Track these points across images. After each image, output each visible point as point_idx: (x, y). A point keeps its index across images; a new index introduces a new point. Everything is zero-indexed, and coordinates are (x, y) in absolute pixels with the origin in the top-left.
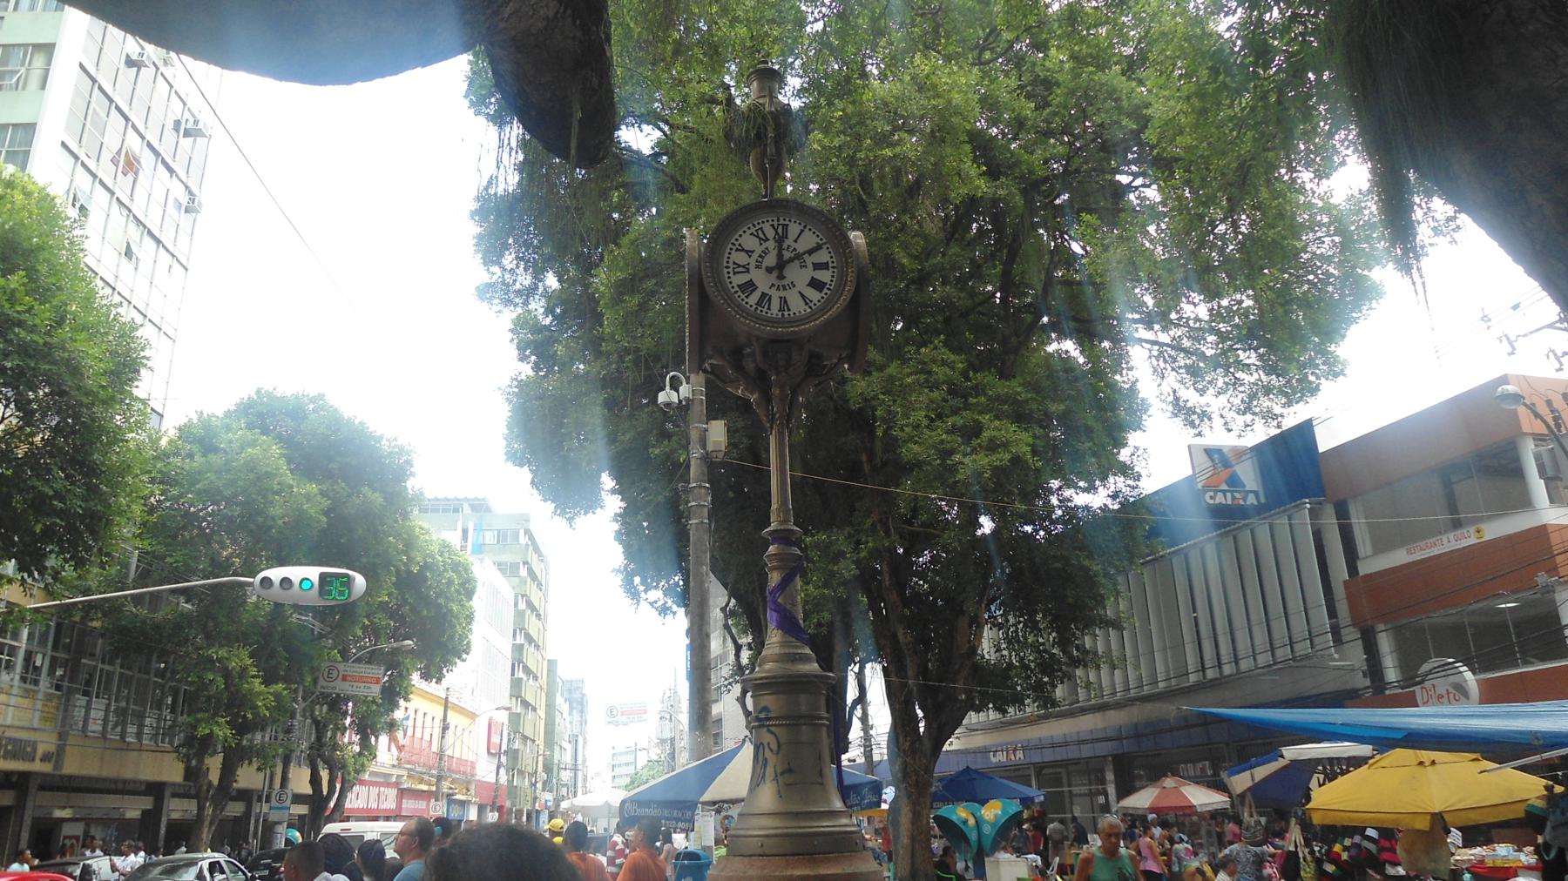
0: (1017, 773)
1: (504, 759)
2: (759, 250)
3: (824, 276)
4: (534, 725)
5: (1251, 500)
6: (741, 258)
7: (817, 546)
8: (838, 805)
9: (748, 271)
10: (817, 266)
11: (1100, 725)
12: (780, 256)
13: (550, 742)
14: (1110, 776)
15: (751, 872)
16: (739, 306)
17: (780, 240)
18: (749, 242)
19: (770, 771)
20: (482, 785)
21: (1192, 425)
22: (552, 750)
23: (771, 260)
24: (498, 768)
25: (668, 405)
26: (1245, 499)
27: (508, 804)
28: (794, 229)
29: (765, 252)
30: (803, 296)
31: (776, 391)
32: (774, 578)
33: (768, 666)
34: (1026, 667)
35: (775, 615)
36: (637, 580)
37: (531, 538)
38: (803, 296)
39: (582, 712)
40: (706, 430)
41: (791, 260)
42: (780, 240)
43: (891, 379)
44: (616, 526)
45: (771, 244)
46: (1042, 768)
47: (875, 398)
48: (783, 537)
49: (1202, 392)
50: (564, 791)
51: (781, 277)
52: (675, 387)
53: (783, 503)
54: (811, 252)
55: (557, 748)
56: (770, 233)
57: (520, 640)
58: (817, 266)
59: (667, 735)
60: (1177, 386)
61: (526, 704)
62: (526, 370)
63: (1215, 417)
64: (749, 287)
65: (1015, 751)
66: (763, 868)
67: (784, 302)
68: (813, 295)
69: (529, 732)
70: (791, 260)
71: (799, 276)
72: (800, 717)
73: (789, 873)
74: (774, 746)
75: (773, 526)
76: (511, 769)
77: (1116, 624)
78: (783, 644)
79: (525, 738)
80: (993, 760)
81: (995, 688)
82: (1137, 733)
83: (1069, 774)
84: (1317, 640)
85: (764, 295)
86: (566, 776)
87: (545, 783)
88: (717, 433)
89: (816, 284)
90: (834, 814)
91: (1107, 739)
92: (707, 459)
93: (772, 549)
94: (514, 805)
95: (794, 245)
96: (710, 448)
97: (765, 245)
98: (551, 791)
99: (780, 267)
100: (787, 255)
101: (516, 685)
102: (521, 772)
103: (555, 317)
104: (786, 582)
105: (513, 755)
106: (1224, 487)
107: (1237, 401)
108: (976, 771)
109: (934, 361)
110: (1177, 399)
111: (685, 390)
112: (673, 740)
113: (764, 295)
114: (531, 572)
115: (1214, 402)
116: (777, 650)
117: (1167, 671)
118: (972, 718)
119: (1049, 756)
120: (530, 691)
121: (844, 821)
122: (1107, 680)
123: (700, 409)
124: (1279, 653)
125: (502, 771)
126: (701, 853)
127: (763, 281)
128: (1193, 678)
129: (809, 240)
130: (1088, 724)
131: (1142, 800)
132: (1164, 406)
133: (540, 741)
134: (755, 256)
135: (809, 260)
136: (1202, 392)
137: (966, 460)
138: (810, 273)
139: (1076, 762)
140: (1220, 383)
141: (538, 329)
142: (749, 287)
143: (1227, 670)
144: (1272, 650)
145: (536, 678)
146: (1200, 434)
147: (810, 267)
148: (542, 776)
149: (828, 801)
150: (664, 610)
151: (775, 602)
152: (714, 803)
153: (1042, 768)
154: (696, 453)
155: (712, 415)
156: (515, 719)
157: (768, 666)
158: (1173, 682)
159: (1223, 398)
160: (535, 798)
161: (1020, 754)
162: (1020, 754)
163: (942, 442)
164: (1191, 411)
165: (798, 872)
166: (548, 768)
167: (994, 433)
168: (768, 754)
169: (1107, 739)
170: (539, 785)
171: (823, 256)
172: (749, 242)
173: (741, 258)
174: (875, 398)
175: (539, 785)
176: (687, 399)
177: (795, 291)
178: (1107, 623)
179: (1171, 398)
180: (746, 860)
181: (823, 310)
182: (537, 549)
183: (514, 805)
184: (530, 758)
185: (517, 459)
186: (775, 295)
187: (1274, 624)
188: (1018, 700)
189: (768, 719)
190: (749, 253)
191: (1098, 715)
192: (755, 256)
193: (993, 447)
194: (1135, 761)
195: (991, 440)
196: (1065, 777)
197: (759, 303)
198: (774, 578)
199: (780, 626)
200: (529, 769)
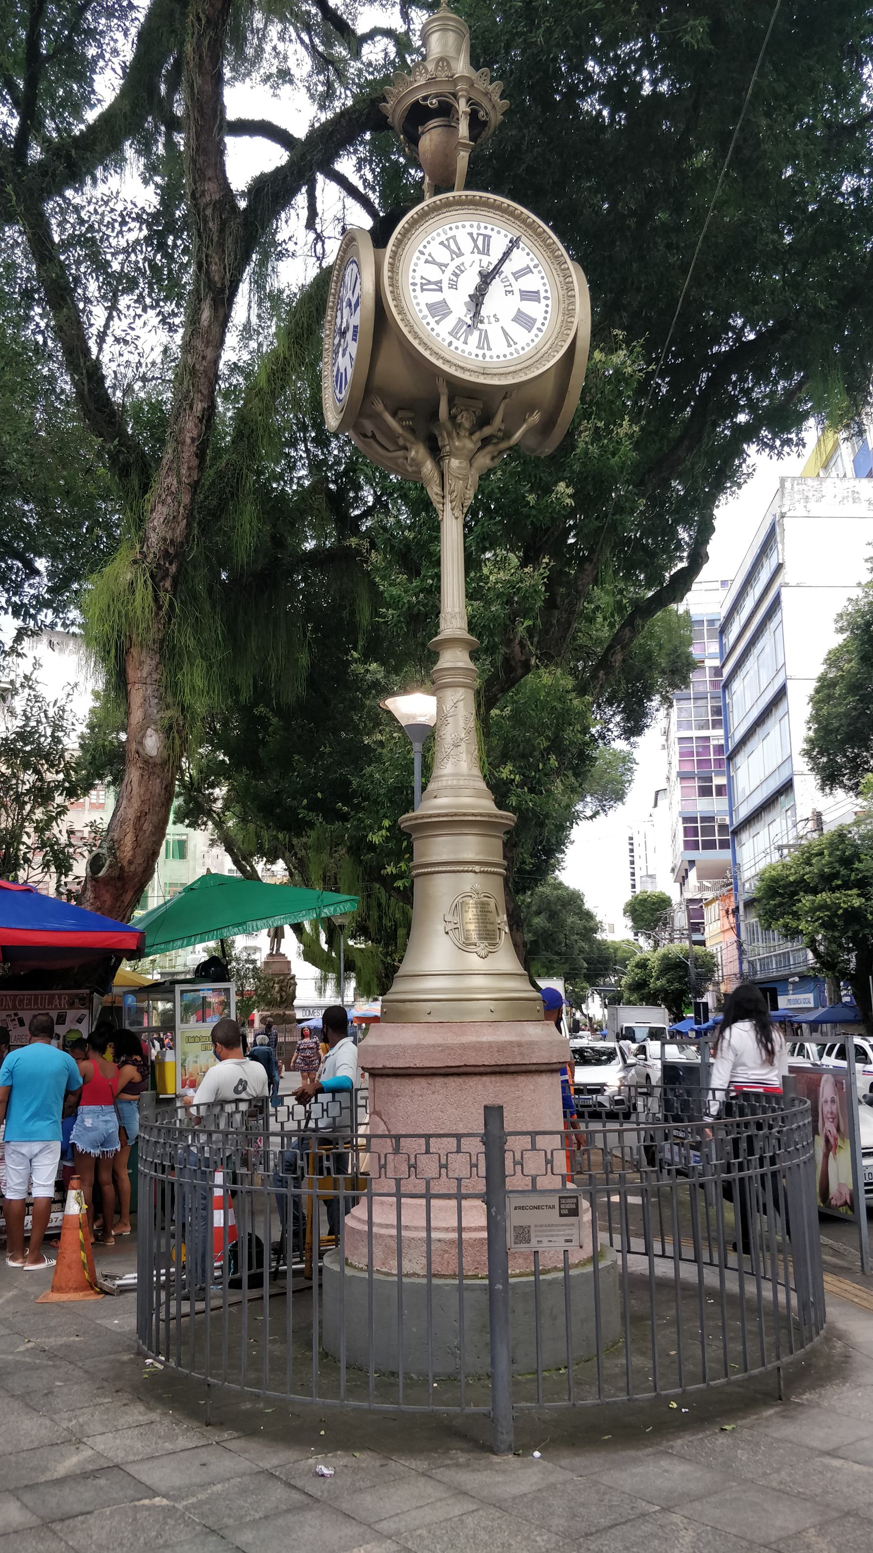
9: (441, 290)
30: (506, 334)
38: (506, 334)
190: (442, 266)
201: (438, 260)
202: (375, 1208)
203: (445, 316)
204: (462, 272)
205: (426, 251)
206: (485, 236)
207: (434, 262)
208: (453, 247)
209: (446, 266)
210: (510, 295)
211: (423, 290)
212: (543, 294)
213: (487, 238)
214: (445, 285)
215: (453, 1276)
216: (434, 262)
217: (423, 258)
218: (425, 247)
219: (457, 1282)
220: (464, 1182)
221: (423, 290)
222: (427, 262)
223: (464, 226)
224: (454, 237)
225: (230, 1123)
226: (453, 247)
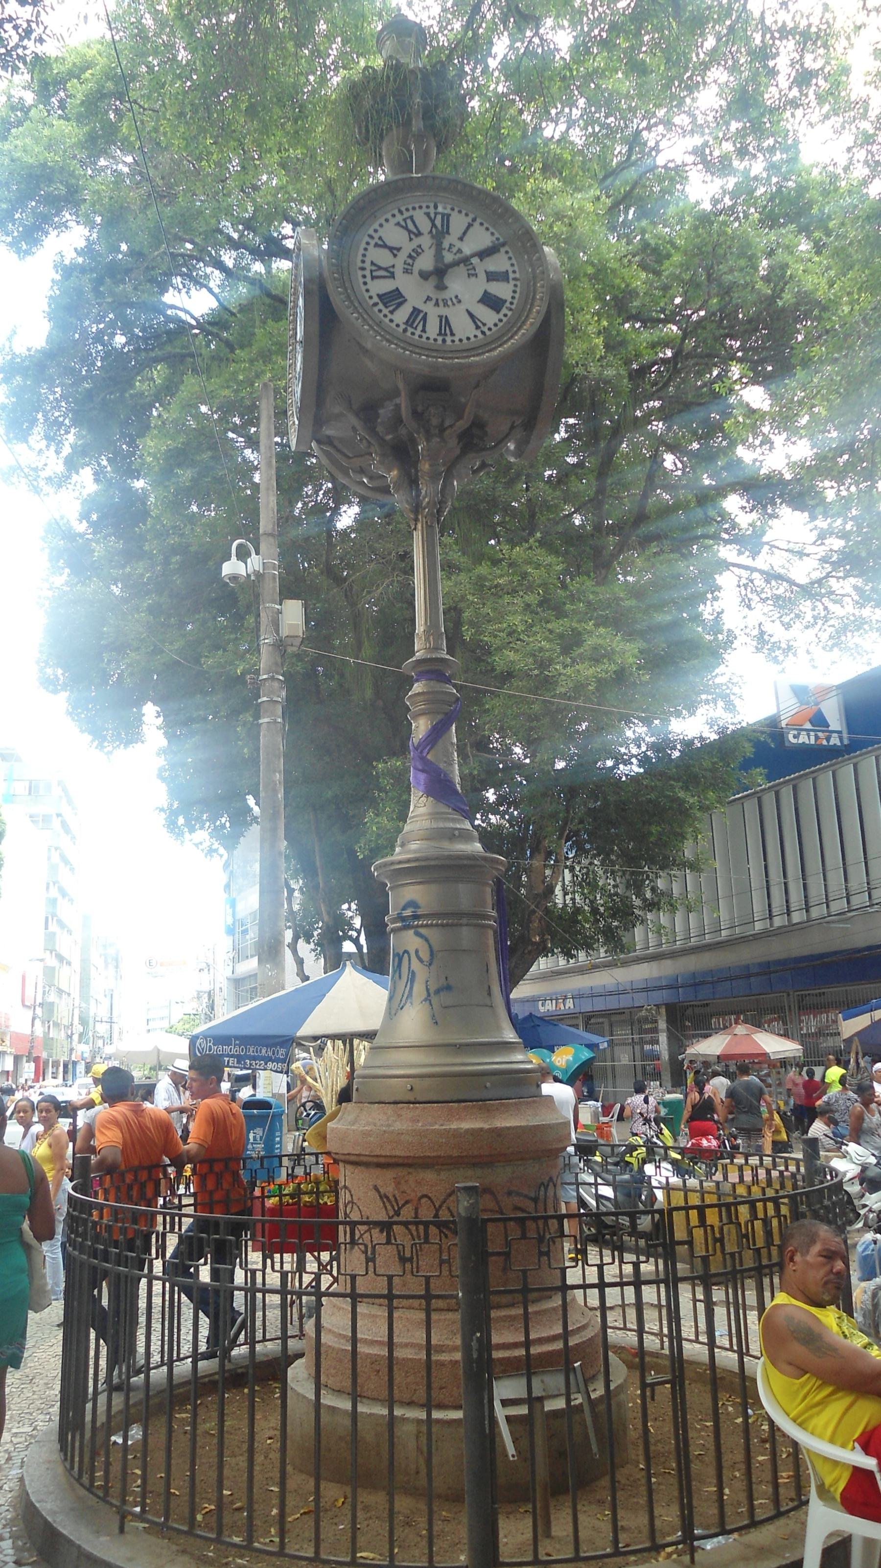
0: (589, 1020)
1: (39, 1011)
2: (408, 247)
3: (502, 290)
4: (68, 978)
5: (835, 741)
6: (383, 258)
7: (389, 773)
8: (510, 1035)
9: (392, 276)
10: (491, 277)
11: (655, 974)
12: (439, 256)
13: (85, 995)
14: (662, 1025)
15: (398, 1126)
16: (379, 324)
17: (439, 234)
18: (394, 235)
19: (419, 988)
20: (17, 1037)
21: (775, 660)
22: (87, 1001)
23: (426, 262)
24: (33, 1019)
25: (234, 578)
26: (828, 739)
27: (44, 1055)
28: (458, 222)
29: (417, 252)
30: (471, 316)
31: (425, 466)
32: (420, 728)
33: (414, 846)
34: (595, 911)
35: (422, 777)
36: (181, 820)
37: (64, 790)
38: (471, 316)
39: (117, 967)
40: (280, 612)
41: (456, 264)
42: (439, 234)
43: (481, 578)
44: (161, 762)
45: (426, 241)
46: (590, 1018)
47: (463, 598)
48: (433, 670)
49: (788, 626)
50: (100, 1043)
51: (441, 287)
52: (243, 555)
53: (432, 626)
54: (483, 254)
55: (92, 1002)
56: (425, 225)
57: (54, 892)
58: (491, 277)
59: (207, 988)
60: (763, 619)
61: (60, 958)
62: (62, 579)
63: (801, 652)
64: (394, 298)
65: (565, 998)
66: (415, 1120)
67: (445, 323)
68: (489, 316)
69: (64, 986)
70: (456, 264)
71: (465, 289)
72: (461, 915)
73: (454, 1126)
74: (425, 955)
75: (419, 655)
76: (46, 1021)
77: (694, 866)
78: (435, 816)
79: (60, 992)
80: (542, 1009)
81: (566, 934)
82: (696, 982)
83: (611, 1026)
84: (852, 898)
85: (416, 311)
86: (102, 1029)
87: (81, 1035)
88: (293, 614)
89: (491, 302)
90: (506, 1046)
91: (660, 988)
92: (280, 646)
93: (418, 687)
94: (50, 1055)
95: (458, 244)
96: (285, 632)
97: (417, 241)
98: (86, 1043)
99: (439, 274)
100: (449, 258)
101: (50, 938)
102: (57, 1025)
103: (92, 524)
104: (437, 733)
105: (48, 1008)
106: (808, 726)
107: (824, 636)
108: (541, 1019)
109: (529, 563)
110: (762, 633)
111: (255, 562)
112: (210, 995)
113: (416, 311)
114: (64, 824)
115: (800, 636)
116: (426, 824)
117: (732, 919)
118: (543, 964)
119: (600, 1005)
120: (64, 944)
121: (519, 1057)
122: (680, 926)
123: (271, 587)
124: (856, 901)
125: (38, 1022)
126: (272, 1101)
127: (415, 293)
128: (758, 926)
129: (480, 239)
130: (641, 973)
131: (712, 1046)
132: (748, 640)
133: (75, 994)
134: (403, 256)
135: (482, 266)
136: (788, 626)
137: (569, 670)
138: (480, 286)
139: (620, 1012)
140: (809, 617)
141: (70, 536)
142: (394, 298)
143: (796, 917)
144: (789, 913)
145: (70, 932)
146: (783, 671)
147: (482, 276)
148: (78, 1028)
149: (499, 1029)
150: (211, 851)
151: (423, 759)
152: (315, 1038)
153: (590, 1018)
154: (267, 639)
155: (288, 592)
156: (50, 973)
157: (414, 846)
158: (737, 930)
159: (811, 632)
160: (72, 1050)
161: (570, 1004)
162: (570, 1004)
163: (541, 649)
164: (776, 646)
165: (466, 1125)
166: (83, 1021)
167: (600, 641)
168: (416, 964)
169: (660, 988)
170: (76, 1037)
171: (499, 263)
172: (394, 235)
173: (383, 258)
174: (463, 598)
175: (76, 1037)
176: (257, 574)
177: (462, 307)
178: (685, 865)
179: (756, 632)
180: (390, 1109)
181: (499, 339)
182: (70, 802)
183: (50, 1055)
184: (64, 1011)
185: (51, 685)
186: (433, 313)
187: (810, 881)
188: (588, 945)
189: (416, 917)
190: (394, 251)
191: (654, 965)
192: (403, 256)
193: (596, 658)
194: (690, 1012)
195: (595, 648)
196: (607, 1027)
197: (410, 322)
198: (420, 728)
199: (430, 792)
200: (65, 1022)
201: (387, 251)
202: (581, 1517)
203: (399, 305)
204: (418, 254)
205: (376, 236)
206: (443, 215)
207: (385, 246)
208: (411, 226)
209: (399, 249)
210: (473, 279)
211: (373, 278)
212: (511, 275)
213: (446, 218)
214: (398, 271)
215: (264, 1283)
216: (385, 246)
217: (372, 242)
218: (376, 231)
219: (423, 1415)
220: (396, 1280)
221: (373, 278)
222: (376, 245)
223: (391, 321)
224: (411, 218)
225: (755, 1175)
226: (411, 226)
